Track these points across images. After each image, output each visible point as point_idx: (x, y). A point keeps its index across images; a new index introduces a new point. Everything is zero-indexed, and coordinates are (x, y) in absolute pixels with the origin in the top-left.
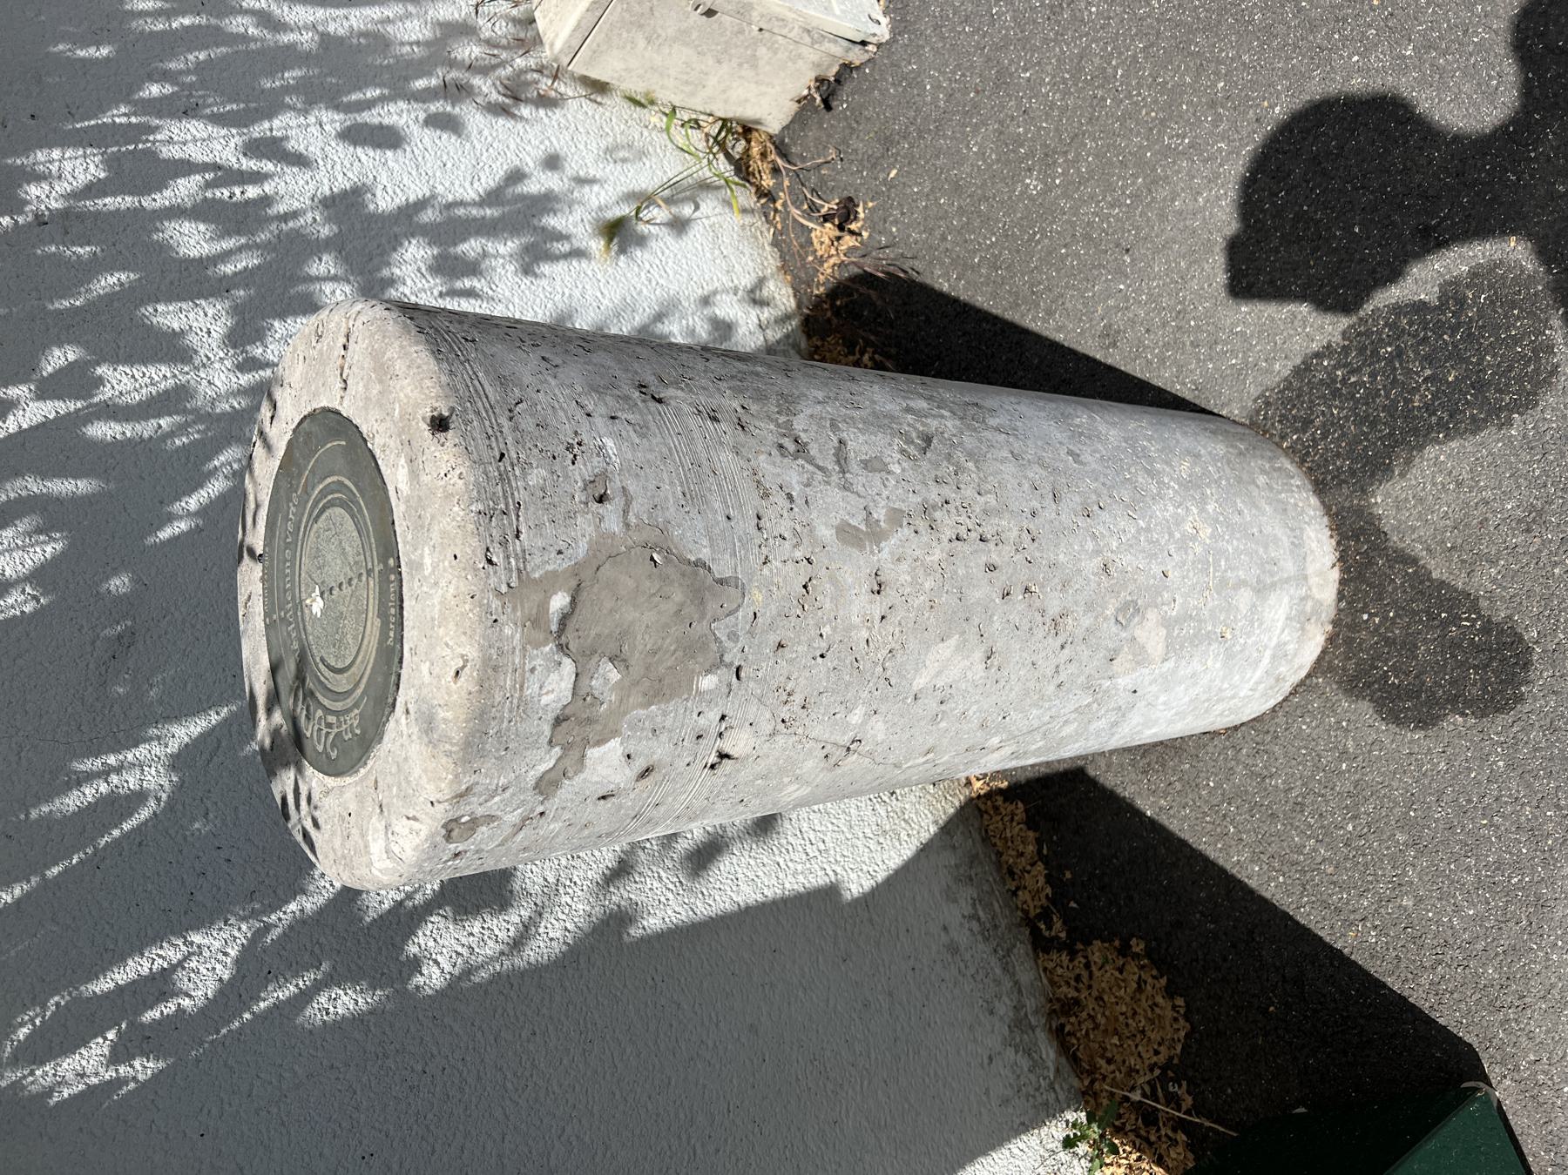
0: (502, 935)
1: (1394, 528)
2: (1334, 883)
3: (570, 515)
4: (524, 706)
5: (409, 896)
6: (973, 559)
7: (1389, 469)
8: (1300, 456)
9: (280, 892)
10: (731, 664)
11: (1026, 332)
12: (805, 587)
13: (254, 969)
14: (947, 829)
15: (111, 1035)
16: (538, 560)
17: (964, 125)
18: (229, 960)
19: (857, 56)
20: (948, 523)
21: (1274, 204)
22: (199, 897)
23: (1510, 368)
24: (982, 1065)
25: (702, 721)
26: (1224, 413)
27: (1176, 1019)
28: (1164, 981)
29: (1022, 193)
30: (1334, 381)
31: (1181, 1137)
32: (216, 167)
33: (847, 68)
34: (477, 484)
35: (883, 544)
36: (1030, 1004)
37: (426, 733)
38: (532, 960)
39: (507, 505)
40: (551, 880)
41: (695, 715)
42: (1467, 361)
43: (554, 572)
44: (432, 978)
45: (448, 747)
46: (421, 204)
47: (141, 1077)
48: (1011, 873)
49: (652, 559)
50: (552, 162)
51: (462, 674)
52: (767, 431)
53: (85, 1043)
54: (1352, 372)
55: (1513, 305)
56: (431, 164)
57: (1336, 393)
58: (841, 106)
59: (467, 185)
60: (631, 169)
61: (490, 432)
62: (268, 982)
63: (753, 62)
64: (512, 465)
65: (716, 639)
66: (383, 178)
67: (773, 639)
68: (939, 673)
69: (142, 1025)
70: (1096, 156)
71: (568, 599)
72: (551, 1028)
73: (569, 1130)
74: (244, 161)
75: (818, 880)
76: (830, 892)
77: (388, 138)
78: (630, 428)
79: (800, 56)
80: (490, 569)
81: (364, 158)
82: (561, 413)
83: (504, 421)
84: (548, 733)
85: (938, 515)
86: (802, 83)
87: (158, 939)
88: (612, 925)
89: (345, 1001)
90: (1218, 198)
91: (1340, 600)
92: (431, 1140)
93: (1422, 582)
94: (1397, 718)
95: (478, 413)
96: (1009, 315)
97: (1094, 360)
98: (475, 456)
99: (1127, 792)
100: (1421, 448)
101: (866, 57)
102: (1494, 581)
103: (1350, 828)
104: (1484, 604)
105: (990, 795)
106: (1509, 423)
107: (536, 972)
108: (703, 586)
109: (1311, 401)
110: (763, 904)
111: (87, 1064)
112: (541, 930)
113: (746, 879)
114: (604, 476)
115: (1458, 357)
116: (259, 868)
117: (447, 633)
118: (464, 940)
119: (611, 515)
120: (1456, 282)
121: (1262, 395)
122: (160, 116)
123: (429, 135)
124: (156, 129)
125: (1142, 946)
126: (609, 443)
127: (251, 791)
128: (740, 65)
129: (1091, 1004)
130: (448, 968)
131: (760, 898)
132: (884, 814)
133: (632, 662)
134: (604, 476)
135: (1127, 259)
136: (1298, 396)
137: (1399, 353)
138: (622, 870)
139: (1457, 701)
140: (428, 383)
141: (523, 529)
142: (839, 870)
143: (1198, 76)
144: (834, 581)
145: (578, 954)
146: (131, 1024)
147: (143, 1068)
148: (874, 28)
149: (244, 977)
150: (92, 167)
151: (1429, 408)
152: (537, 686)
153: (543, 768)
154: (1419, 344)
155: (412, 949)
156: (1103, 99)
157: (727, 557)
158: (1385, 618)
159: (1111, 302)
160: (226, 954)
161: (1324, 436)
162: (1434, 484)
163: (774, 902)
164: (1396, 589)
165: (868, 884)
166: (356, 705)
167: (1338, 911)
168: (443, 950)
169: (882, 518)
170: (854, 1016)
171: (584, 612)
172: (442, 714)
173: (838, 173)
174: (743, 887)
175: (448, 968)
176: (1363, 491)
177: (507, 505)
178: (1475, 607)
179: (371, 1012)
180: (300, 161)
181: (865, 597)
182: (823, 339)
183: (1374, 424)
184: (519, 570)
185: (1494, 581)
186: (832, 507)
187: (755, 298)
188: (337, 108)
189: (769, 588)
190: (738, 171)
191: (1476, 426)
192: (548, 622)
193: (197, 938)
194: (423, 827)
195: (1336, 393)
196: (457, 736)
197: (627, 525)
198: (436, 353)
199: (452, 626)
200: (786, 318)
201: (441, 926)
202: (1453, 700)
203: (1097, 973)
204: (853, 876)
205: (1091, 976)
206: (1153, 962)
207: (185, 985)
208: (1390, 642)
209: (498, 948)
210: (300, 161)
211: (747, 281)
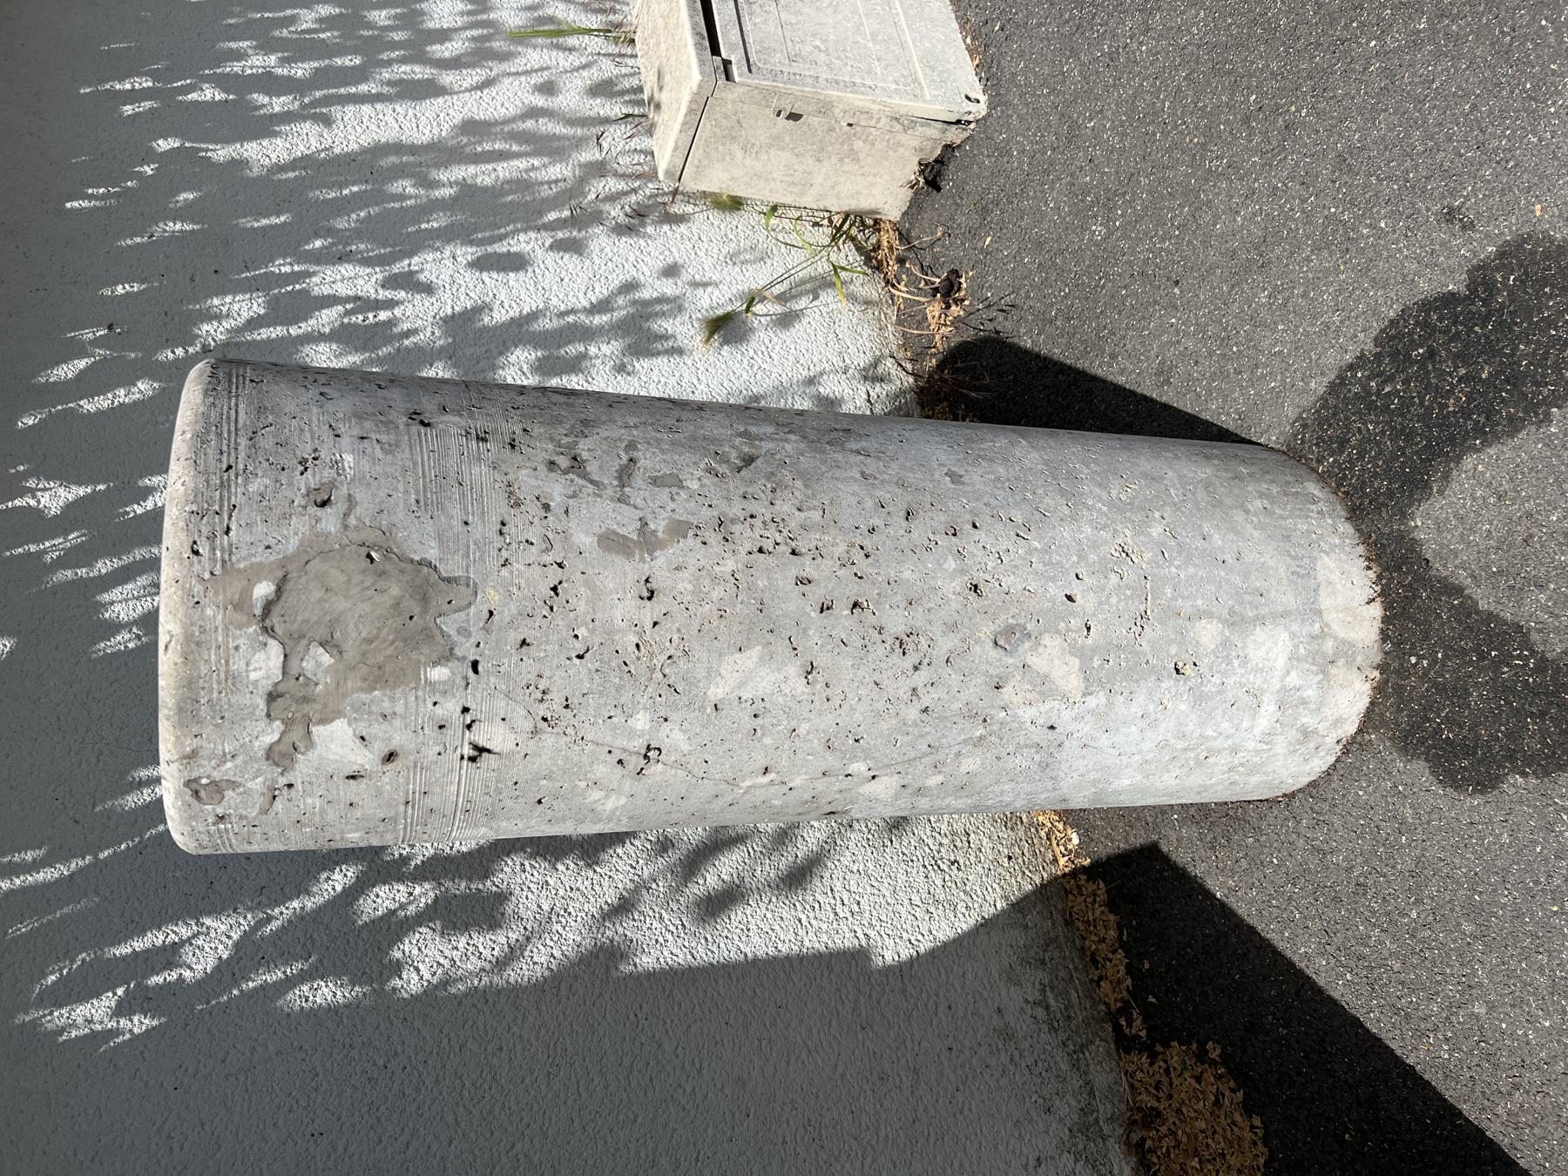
0: (486, 953)
1: (1436, 554)
2: (1402, 983)
3: (286, 517)
4: (233, 680)
5: (402, 907)
6: (778, 576)
7: (1426, 486)
8: (1335, 481)
9: (287, 890)
10: (464, 658)
11: (1094, 378)
12: (554, 589)
13: (249, 953)
14: (1019, 907)
15: (120, 992)
16: (244, 553)
17: (1043, 184)
19: (955, 136)
20: (747, 538)
21: (1303, 212)
22: (216, 886)
23: (1545, 357)
24: (1025, 1167)
25: (438, 710)
26: (1262, 441)
27: (1255, 1143)
28: (1240, 1095)
30: (1369, 394)
32: (357, 298)
33: (949, 148)
35: (657, 553)
36: (1104, 1109)
38: (512, 980)
39: (221, 507)
40: (546, 907)
41: (430, 705)
42: (1500, 353)
43: (260, 564)
44: (411, 983)
46: (534, 316)
47: (136, 1030)
48: (1094, 961)
49: (369, 556)
50: (671, 271)
52: (542, 450)
53: (98, 995)
54: (1385, 382)
55: (1545, 282)
56: (549, 280)
57: (1371, 407)
58: (947, 186)
59: (581, 295)
60: (750, 270)
61: (225, 448)
62: (260, 964)
63: (853, 156)
65: (443, 633)
66: (502, 296)
67: (514, 637)
68: (742, 685)
69: (147, 987)
70: (1150, 192)
71: (273, 588)
72: (519, 1046)
73: (519, 1146)
74: (381, 291)
75: (849, 942)
76: (857, 958)
77: (516, 263)
78: (378, 447)
79: (899, 144)
81: (487, 280)
83: (243, 442)
85: (736, 528)
86: (910, 171)
87: (174, 919)
88: (601, 962)
89: (326, 993)
90: (1255, 214)
91: (1384, 640)
92: (379, 1131)
93: (1469, 616)
94: (1455, 781)
95: (220, 435)
97: (1152, 400)
99: (1198, 870)
100: (1458, 459)
101: (966, 134)
102: (1545, 609)
103: (1414, 915)
104: (1535, 636)
105: (1074, 874)
106: (1548, 419)
107: (515, 991)
108: (428, 587)
109: (1347, 418)
110: (775, 958)
111: (96, 1012)
112: (527, 954)
113: (764, 930)
114: (332, 485)
115: (1491, 351)
116: (272, 868)
118: (447, 953)
119: (329, 520)
120: (1483, 267)
121: (1300, 417)
122: (318, 263)
123: (551, 258)
124: (314, 274)
125: (1218, 1052)
126: (349, 459)
128: (841, 160)
129: (1172, 1118)
130: (427, 976)
131: (771, 951)
132: (939, 882)
133: (347, 647)
134: (332, 485)
135: (1176, 291)
136: (1334, 415)
137: (1432, 353)
138: (624, 907)
139: (1517, 759)
142: (872, 933)
143: (1232, 94)
144: (590, 585)
145: (560, 980)
146: (138, 985)
147: (140, 1024)
148: (972, 107)
150: (255, 306)
151: (1465, 413)
154: (1451, 341)
155: (397, 954)
156: (1154, 134)
157: (458, 557)
158: (1434, 661)
159: (1165, 338)
160: (229, 937)
161: (1361, 456)
162: (1474, 499)
163: (787, 957)
164: (1443, 625)
165: (906, 953)
168: (426, 959)
169: (661, 529)
170: (866, 1087)
171: (289, 599)
174: (755, 939)
175: (427, 976)
176: (1404, 515)
177: (221, 507)
178: (1526, 643)
179: (346, 1006)
180: (428, 289)
181: (631, 603)
183: (1410, 436)
184: (224, 561)
185: (1545, 609)
186: (594, 516)
187: (871, 375)
188: (471, 243)
189: (508, 587)
190: (868, 260)
191: (1515, 426)
192: (251, 606)
193: (208, 921)
195: (1371, 407)
197: (346, 527)
200: (902, 392)
201: (428, 937)
202: (1511, 756)
203: (1176, 1082)
204: (889, 942)
205: (1171, 1084)
206: (1230, 1071)
207: (189, 959)
208: (1442, 689)
209: (480, 964)
210: (428, 289)
211: (863, 360)
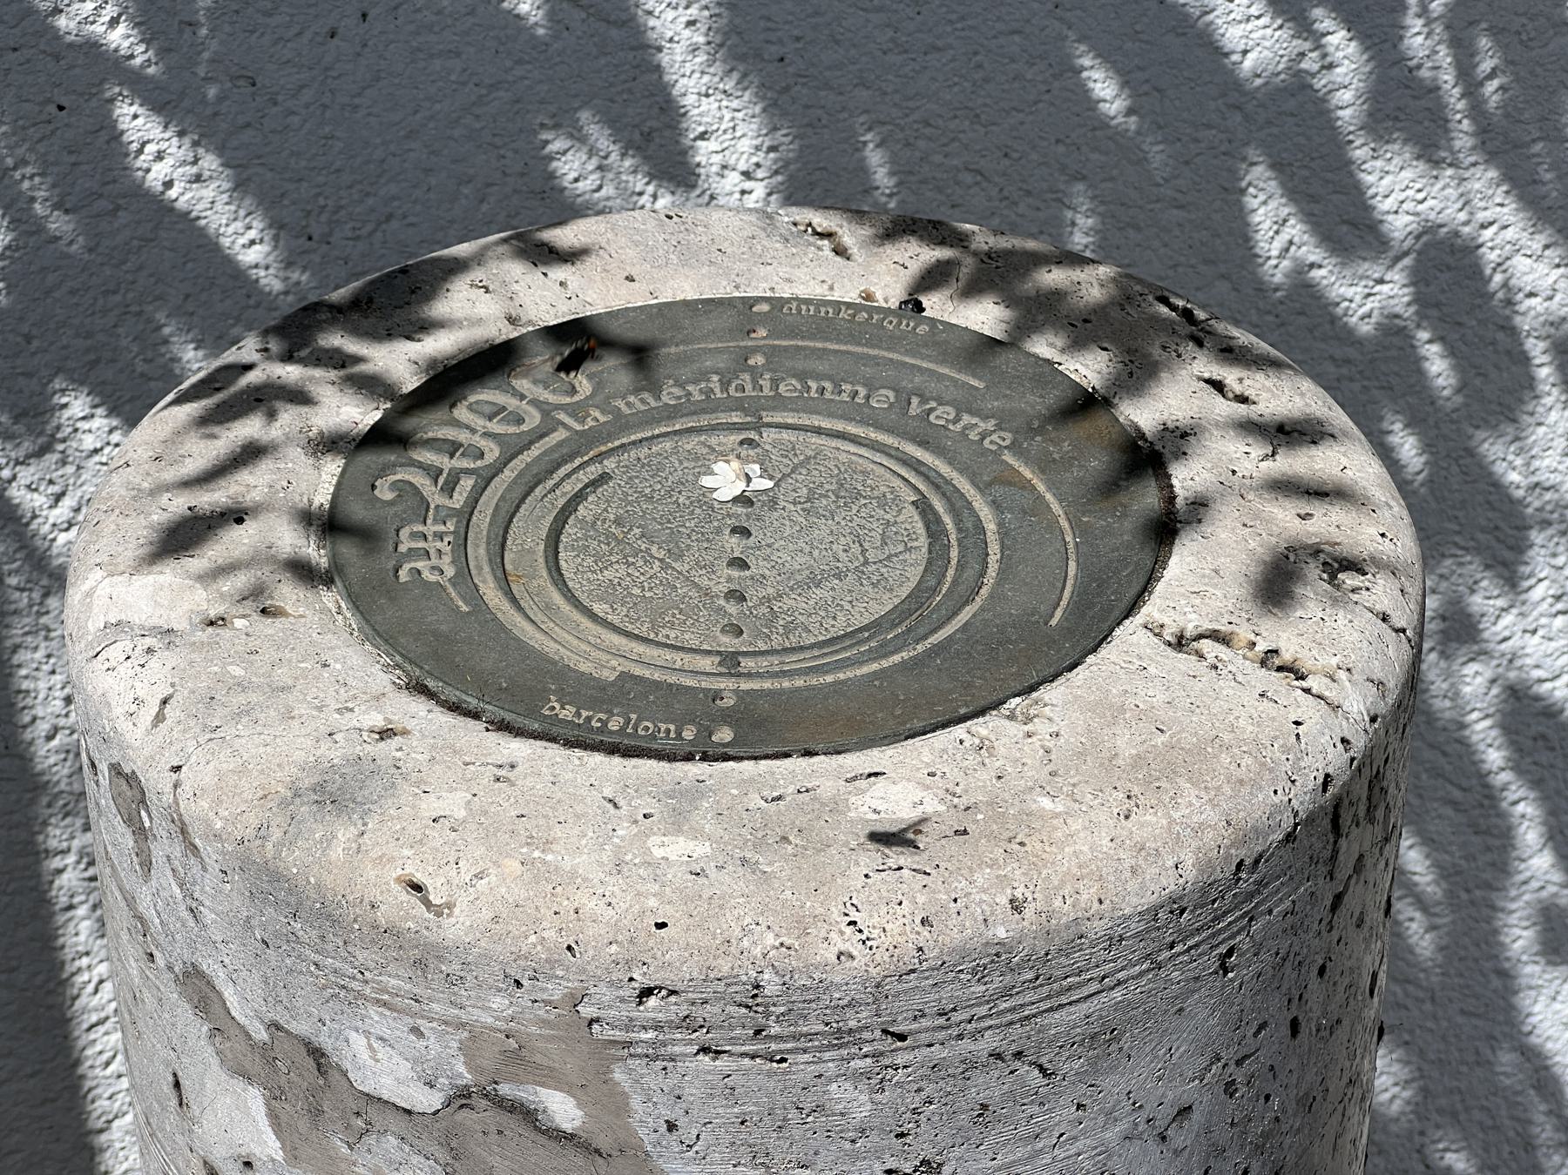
4: (345, 995)
18: (99, 29)
34: (826, 987)
37: (319, 788)
39: (778, 1038)
45: (276, 834)
51: (412, 899)
61: (956, 1017)
64: (876, 1055)
71: (567, 1127)
80: (630, 992)
82: (1020, 1153)
83: (990, 1041)
84: (294, 1027)
95: (1007, 993)
98: (891, 986)
116: (307, 96)
117: (506, 880)
127: (493, 87)
140: (1088, 894)
141: (723, 1063)
149: (57, 58)
152: (387, 1033)
153: (229, 993)
166: (464, 574)
171: (542, 1154)
172: (344, 834)
177: (778, 1038)
184: (628, 1044)
194: (140, 732)
196: (293, 861)
198: (1177, 906)
199: (519, 893)
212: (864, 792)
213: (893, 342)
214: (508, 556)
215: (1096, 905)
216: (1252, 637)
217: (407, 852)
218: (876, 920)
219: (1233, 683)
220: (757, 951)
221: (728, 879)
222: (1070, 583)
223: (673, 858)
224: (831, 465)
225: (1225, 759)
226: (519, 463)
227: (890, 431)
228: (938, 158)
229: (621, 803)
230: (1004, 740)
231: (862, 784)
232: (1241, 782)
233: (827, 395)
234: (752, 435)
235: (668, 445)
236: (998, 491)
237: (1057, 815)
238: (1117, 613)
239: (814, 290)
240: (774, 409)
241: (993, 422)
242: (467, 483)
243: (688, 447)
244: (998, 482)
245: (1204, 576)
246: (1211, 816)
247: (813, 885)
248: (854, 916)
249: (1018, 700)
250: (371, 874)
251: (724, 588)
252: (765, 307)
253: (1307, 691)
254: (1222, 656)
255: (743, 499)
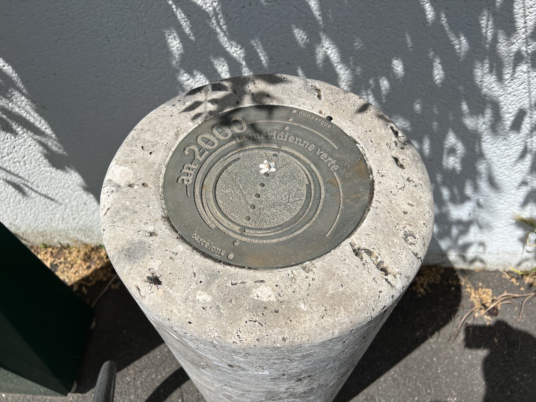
29: (452, 394)
31: (105, 279)
96: (403, 362)
116: (238, 19)
167: (141, 372)
173: (512, 315)
182: (441, 275)
199: (160, 301)
212: (258, 287)
213: (320, 129)
214: (206, 179)
215: (307, 341)
216: (378, 255)
217: (139, 279)
218: (245, 336)
219: (367, 272)
220: (212, 336)
221: (211, 313)
222: (336, 222)
223: (201, 300)
224: (292, 166)
225: (356, 302)
226: (214, 155)
227: (309, 159)
228: (368, 51)
229: (196, 276)
230: (300, 278)
231: (258, 284)
232: (358, 311)
233: (299, 144)
234: (277, 153)
235: (257, 151)
236: (329, 185)
237: (304, 312)
238: (344, 237)
239: (307, 108)
240: (285, 145)
241: (335, 161)
242: (207, 153)
243: (261, 153)
244: (331, 183)
245: (372, 229)
246: (347, 320)
247: (231, 321)
248: (239, 334)
249: (309, 262)
250: (130, 281)
251: (251, 202)
252: (295, 111)
253: (386, 280)
254: (368, 261)
255: (267, 174)
